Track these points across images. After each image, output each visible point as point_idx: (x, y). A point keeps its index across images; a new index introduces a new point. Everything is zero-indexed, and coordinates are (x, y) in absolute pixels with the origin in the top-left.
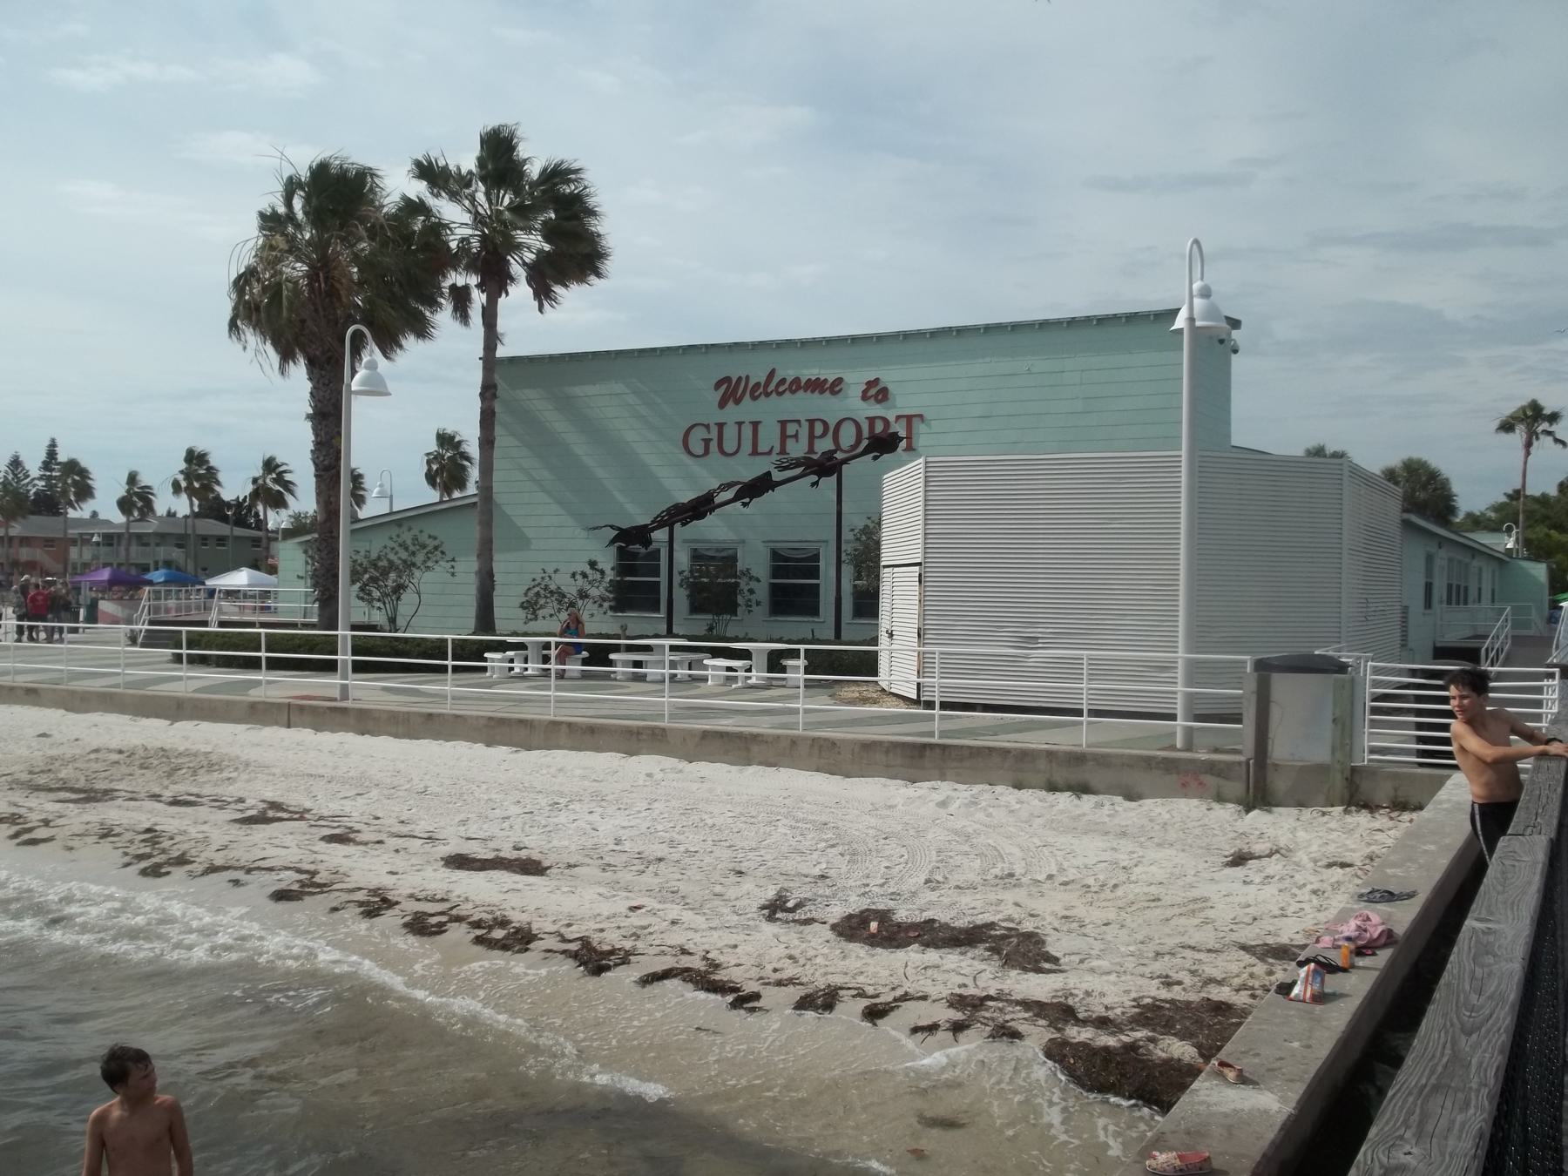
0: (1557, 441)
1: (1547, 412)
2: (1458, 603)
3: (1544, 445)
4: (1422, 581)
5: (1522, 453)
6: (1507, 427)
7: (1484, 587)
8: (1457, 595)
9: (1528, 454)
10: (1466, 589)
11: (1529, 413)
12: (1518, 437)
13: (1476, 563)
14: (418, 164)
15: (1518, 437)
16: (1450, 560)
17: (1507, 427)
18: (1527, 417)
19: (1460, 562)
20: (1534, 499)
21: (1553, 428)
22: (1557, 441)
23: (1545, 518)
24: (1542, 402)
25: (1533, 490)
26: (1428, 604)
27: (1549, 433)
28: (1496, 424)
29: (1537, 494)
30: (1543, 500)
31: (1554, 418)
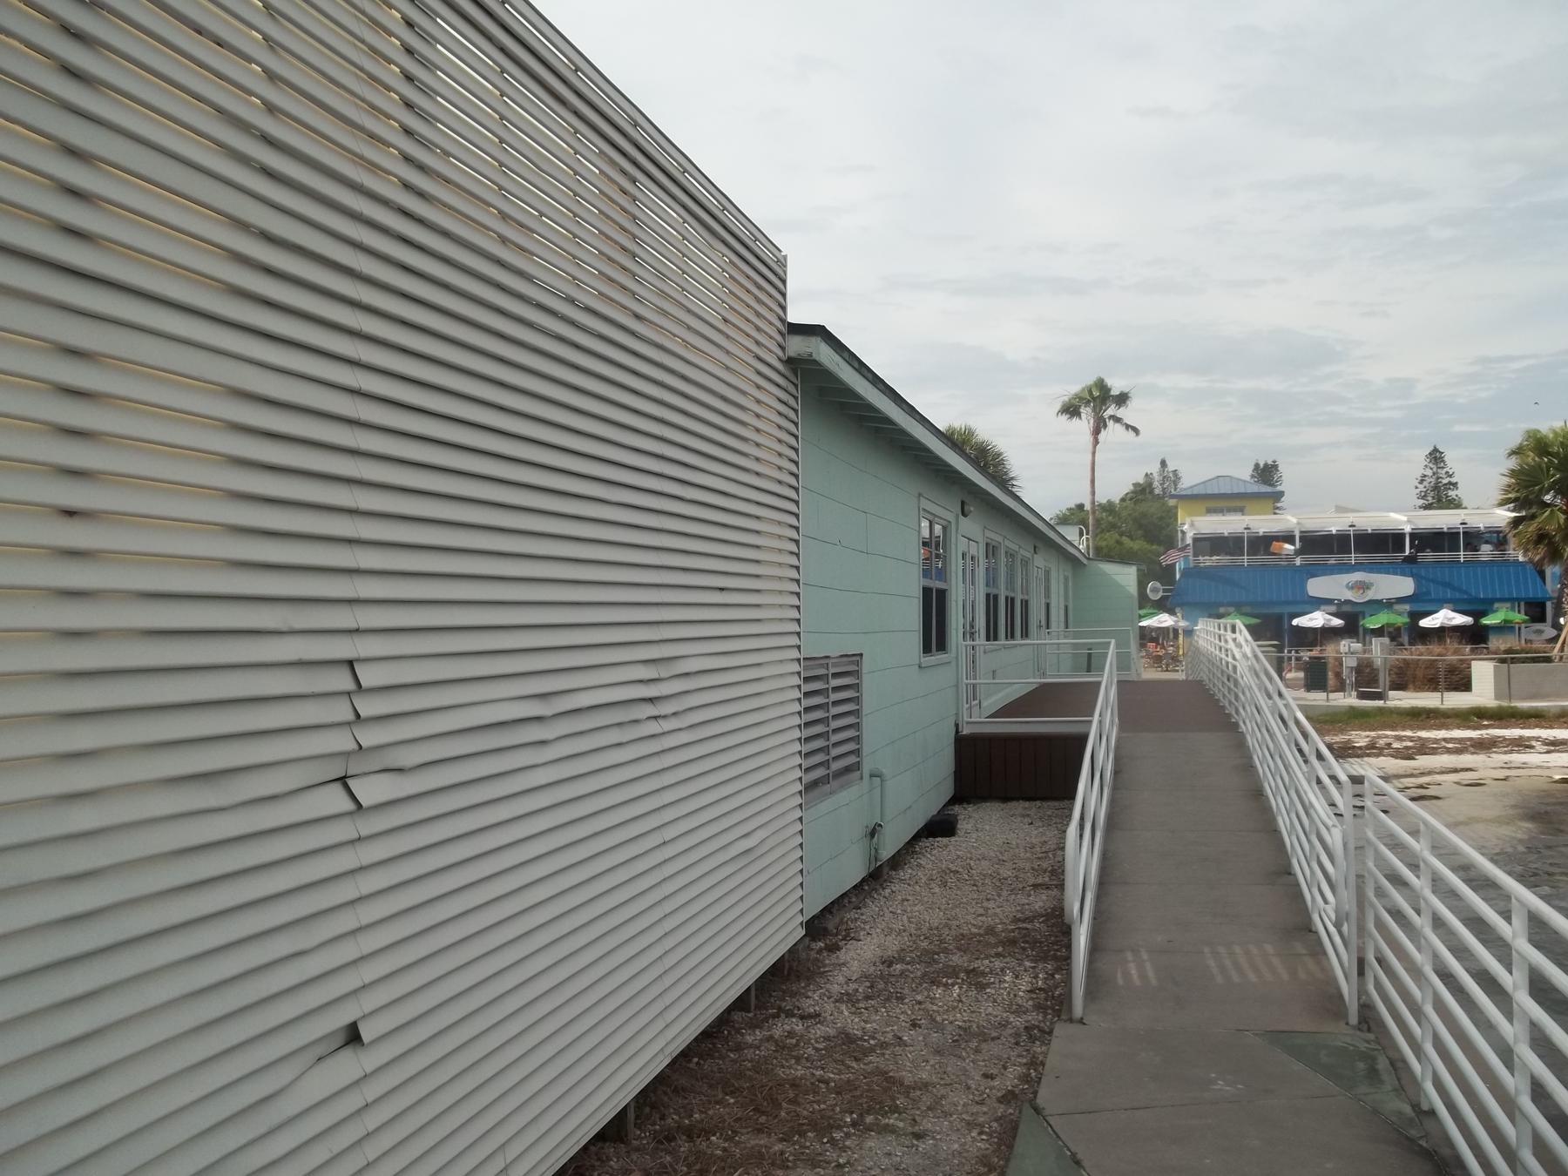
0: (1128, 427)
1: (1115, 392)
2: (1011, 635)
3: (1113, 432)
4: (913, 585)
5: (1089, 439)
6: (1071, 410)
7: (1053, 605)
8: (1006, 618)
9: (1096, 442)
10: (1025, 604)
11: (1096, 393)
12: (1084, 424)
13: (1040, 561)
14: (1436, 450)
15: (1084, 424)
16: (991, 550)
17: (1071, 410)
18: (1094, 399)
19: (1011, 555)
20: (1103, 508)
21: (1121, 413)
22: (1128, 427)
23: (1113, 526)
24: (1109, 382)
25: (1102, 498)
26: (934, 635)
27: (1118, 420)
28: (1058, 406)
29: (1104, 501)
30: (1109, 508)
31: (1122, 399)
